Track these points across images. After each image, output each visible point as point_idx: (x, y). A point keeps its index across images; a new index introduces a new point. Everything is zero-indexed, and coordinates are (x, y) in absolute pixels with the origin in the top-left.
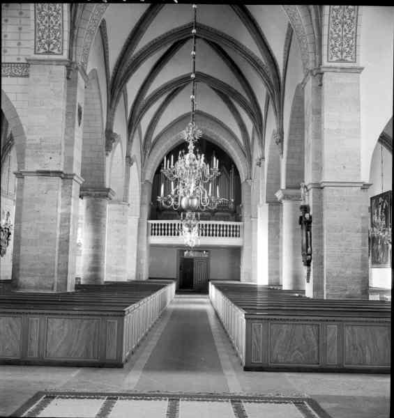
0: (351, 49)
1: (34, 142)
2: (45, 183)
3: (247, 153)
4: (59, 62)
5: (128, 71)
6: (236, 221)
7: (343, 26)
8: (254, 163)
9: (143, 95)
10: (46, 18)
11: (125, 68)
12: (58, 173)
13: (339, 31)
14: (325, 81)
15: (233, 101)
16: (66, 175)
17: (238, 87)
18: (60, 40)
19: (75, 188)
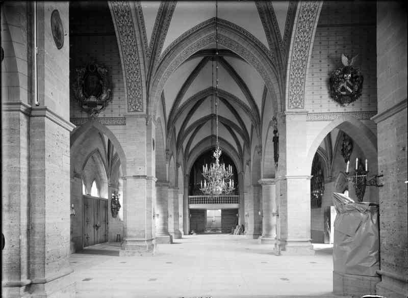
0: (301, 101)
1: (131, 160)
2: (137, 182)
3: (241, 157)
4: (141, 116)
5: (176, 116)
6: (235, 194)
7: (296, 88)
8: (245, 163)
9: (184, 128)
10: (133, 92)
11: (175, 115)
12: (144, 177)
13: (301, 37)
14: (287, 120)
15: (233, 129)
16: (148, 177)
17: (236, 121)
18: (141, 103)
19: (154, 183)
